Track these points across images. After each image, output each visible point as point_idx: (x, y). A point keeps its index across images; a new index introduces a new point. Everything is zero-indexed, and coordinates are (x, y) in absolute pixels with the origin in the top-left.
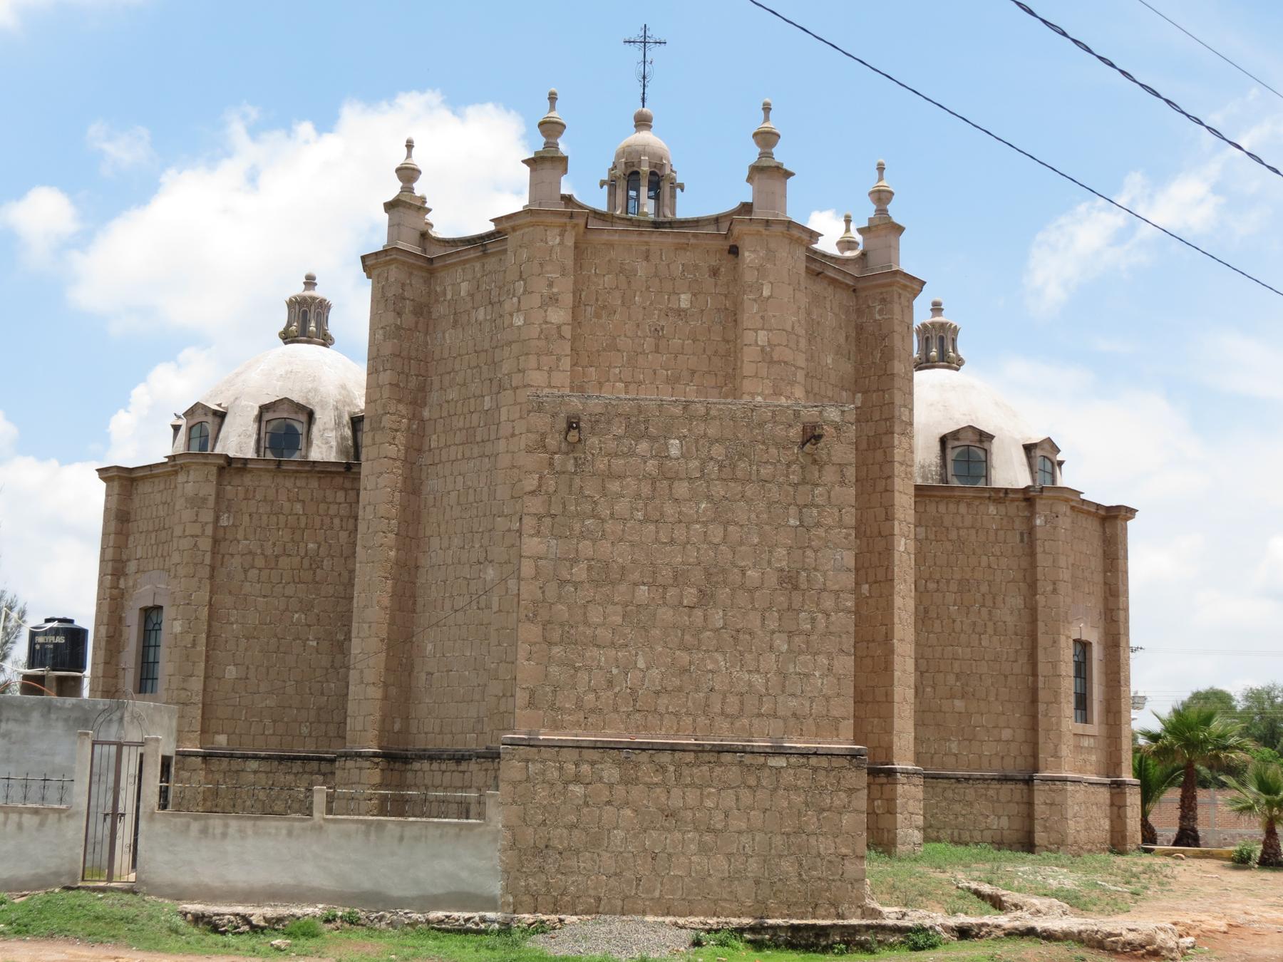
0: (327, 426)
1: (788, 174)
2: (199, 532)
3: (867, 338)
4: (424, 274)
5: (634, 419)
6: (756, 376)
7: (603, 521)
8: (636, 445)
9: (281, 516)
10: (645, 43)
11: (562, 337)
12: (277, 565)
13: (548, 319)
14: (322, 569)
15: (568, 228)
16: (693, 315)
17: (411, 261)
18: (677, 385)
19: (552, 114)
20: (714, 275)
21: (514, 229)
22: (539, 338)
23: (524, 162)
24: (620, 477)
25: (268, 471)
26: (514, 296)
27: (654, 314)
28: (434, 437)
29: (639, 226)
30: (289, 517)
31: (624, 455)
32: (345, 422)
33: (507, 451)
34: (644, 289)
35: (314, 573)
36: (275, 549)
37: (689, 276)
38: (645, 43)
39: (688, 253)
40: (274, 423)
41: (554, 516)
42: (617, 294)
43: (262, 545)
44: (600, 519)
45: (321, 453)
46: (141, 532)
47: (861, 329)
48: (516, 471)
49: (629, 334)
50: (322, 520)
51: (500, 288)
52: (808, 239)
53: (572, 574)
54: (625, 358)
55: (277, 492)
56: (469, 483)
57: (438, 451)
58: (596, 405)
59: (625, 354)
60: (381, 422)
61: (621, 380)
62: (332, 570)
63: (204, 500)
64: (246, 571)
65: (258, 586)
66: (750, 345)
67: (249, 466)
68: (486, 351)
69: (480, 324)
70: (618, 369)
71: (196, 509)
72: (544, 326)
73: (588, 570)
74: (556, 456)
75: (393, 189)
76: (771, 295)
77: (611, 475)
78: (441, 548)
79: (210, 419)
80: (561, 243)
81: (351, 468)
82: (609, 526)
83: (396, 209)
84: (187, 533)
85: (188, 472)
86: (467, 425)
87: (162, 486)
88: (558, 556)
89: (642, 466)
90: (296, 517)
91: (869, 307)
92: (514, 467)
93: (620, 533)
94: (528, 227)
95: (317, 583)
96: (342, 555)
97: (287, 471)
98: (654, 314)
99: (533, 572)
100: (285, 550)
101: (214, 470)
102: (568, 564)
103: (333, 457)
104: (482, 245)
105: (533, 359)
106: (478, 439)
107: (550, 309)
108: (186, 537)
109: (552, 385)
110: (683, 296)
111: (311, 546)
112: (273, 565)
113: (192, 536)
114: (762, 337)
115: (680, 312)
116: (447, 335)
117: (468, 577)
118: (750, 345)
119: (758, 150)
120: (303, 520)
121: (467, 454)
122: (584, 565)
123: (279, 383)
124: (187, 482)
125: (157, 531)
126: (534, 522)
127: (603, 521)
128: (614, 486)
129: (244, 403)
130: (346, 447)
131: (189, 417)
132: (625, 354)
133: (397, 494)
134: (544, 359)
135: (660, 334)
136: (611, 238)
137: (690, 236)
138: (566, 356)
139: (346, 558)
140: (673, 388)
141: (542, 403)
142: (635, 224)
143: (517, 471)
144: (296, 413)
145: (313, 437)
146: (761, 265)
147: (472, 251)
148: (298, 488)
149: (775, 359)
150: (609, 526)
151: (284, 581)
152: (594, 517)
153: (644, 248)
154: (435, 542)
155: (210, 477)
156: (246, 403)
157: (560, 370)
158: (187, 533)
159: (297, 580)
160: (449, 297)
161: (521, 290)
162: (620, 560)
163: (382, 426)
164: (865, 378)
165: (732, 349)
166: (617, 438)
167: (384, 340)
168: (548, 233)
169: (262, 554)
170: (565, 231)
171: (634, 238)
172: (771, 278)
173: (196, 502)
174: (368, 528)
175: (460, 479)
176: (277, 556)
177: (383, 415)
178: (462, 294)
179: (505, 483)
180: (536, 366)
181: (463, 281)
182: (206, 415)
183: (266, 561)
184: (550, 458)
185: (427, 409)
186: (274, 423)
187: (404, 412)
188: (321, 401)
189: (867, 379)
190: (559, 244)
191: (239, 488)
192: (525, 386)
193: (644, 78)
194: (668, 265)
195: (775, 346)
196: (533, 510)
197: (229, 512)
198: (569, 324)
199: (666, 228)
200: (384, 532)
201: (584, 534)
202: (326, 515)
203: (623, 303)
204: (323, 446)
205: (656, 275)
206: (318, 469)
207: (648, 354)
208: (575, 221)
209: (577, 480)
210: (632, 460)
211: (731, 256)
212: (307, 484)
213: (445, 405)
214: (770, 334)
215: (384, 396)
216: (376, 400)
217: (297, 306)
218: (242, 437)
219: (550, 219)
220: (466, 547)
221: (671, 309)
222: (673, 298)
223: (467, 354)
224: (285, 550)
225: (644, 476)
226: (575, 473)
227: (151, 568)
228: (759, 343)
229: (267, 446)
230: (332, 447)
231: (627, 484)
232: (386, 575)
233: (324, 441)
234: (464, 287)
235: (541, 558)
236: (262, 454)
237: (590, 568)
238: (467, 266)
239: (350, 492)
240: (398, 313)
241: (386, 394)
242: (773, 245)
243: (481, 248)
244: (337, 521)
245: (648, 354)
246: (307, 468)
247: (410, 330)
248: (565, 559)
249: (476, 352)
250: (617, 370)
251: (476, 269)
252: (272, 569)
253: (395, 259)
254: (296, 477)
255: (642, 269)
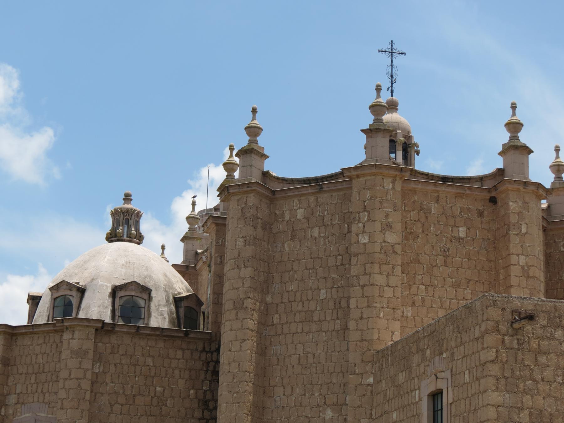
0: (161, 303)
1: (531, 152)
2: (81, 376)
3: (554, 263)
4: (268, 202)
5: (553, 315)
6: (519, 286)
7: (537, 382)
8: (555, 332)
9: (137, 367)
10: (392, 53)
11: (395, 252)
12: (134, 402)
13: (386, 240)
14: (166, 406)
15: (398, 178)
16: (468, 242)
17: (263, 192)
18: (459, 289)
19: (379, 100)
20: (481, 216)
21: (358, 176)
22: (380, 252)
23: (362, 131)
24: (547, 353)
25: (128, 333)
26: (359, 222)
27: (443, 240)
28: (277, 316)
29: (432, 180)
30: (143, 368)
31: (548, 339)
32: (171, 301)
33: (357, 329)
34: (436, 223)
35: (161, 409)
36: (133, 390)
37: (464, 216)
38: (392, 53)
39: (464, 200)
40: (125, 299)
41: (506, 378)
42: (419, 225)
43: (123, 388)
44: (535, 381)
45: (158, 322)
46: (21, 374)
47: (550, 257)
48: (365, 343)
49: (428, 253)
50: (167, 371)
51: (332, 215)
52: (545, 195)
53: (519, 418)
54: (425, 269)
55: (135, 348)
56: (309, 350)
57: (280, 326)
58: (529, 304)
59: (425, 266)
60: (243, 304)
61: (423, 284)
62: (173, 407)
63: (86, 353)
64: (112, 406)
65: (121, 417)
66: (515, 265)
67: (116, 329)
68: (321, 258)
69: (315, 239)
70: (421, 276)
71: (79, 359)
72: (383, 244)
73: (529, 415)
74: (506, 337)
75: (243, 141)
76: (527, 232)
77: (539, 352)
78: (284, 395)
79: (74, 293)
80: (393, 188)
81: (188, 334)
82: (541, 386)
83: (249, 155)
84: (72, 376)
85: (73, 332)
86: (306, 309)
87: (41, 341)
88: (510, 405)
89: (559, 346)
90: (148, 367)
91: (555, 242)
92: (363, 340)
93: (548, 391)
94: (370, 176)
95: (163, 416)
96: (180, 397)
97: (142, 334)
98: (443, 240)
99: (496, 416)
100: (140, 391)
101: (93, 330)
102: (517, 411)
103: (166, 325)
104: (319, 185)
105: (376, 266)
106: (316, 318)
107: (387, 233)
108: (71, 379)
109: (390, 285)
110: (461, 229)
111: (158, 389)
112: (131, 402)
113: (77, 379)
114: (522, 260)
115: (459, 240)
116: (286, 245)
117: (310, 416)
118: (515, 265)
119: (509, 135)
120: (153, 370)
121: (306, 329)
122: (526, 412)
123: (123, 270)
124: (73, 339)
125: (36, 374)
126: (495, 381)
127: (537, 382)
128: (543, 359)
129: (100, 283)
130: (173, 318)
131: (55, 291)
132: (425, 266)
133: (254, 355)
134: (384, 267)
135: (447, 253)
136: (416, 186)
137: (466, 188)
138: (398, 265)
139: (183, 399)
140: (456, 291)
141: (496, 301)
142: (430, 178)
143: (366, 343)
144: (141, 292)
145: (151, 310)
146: (520, 212)
147: (309, 188)
148: (149, 346)
149: (531, 275)
150: (541, 386)
151: (139, 414)
152: (531, 379)
153: (435, 195)
154: (279, 390)
155: (90, 336)
156: (102, 283)
157: (394, 275)
158: (72, 376)
159: (148, 413)
160: (287, 218)
161: (366, 219)
162: (549, 410)
163: (244, 306)
164: (554, 289)
165: (493, 267)
166: (543, 327)
167: (245, 246)
168: (385, 181)
169: (124, 393)
170: (396, 180)
171: (431, 188)
172: (527, 221)
173: (80, 354)
174: (234, 379)
175: (300, 347)
176: (134, 396)
177: (245, 298)
178: (298, 217)
179: (356, 351)
180: (378, 271)
181: (299, 208)
182: (71, 290)
183: (126, 400)
184: (503, 339)
185: (270, 296)
186: (125, 299)
187: (257, 298)
188: (155, 284)
189: (555, 291)
190: (392, 189)
191: (108, 345)
192: (371, 285)
193: (392, 76)
194: (451, 207)
195: (530, 266)
196: (493, 373)
197: (101, 362)
198: (399, 244)
199: (449, 182)
200: (247, 382)
201: (526, 391)
202: (169, 367)
203: (423, 231)
204: (159, 317)
205: (444, 214)
206: (165, 334)
207: (440, 266)
208: (403, 174)
209: (520, 354)
210: (553, 342)
211: (491, 204)
212: (156, 344)
213: (286, 294)
214: (527, 259)
215: (246, 286)
216: (239, 288)
217: (122, 215)
218: (101, 307)
219: (387, 172)
220: (307, 394)
221: (454, 237)
222: (455, 229)
223: (304, 259)
224: (140, 391)
225: (561, 353)
226: (518, 349)
227: (31, 400)
228: (521, 264)
229: (120, 315)
230: (165, 318)
231: (551, 358)
232: (248, 412)
233: (159, 314)
234: (300, 213)
235: (500, 406)
236: (116, 320)
237: (531, 414)
238: (302, 198)
239: (186, 351)
240: (255, 228)
241: (248, 283)
242: (527, 199)
243: (317, 187)
244: (177, 372)
245: (440, 266)
246: (158, 333)
247: (261, 240)
248: (515, 407)
249: (311, 258)
250: (420, 277)
251: (311, 201)
252: (130, 405)
253: (254, 190)
254: (148, 339)
255: (435, 209)
